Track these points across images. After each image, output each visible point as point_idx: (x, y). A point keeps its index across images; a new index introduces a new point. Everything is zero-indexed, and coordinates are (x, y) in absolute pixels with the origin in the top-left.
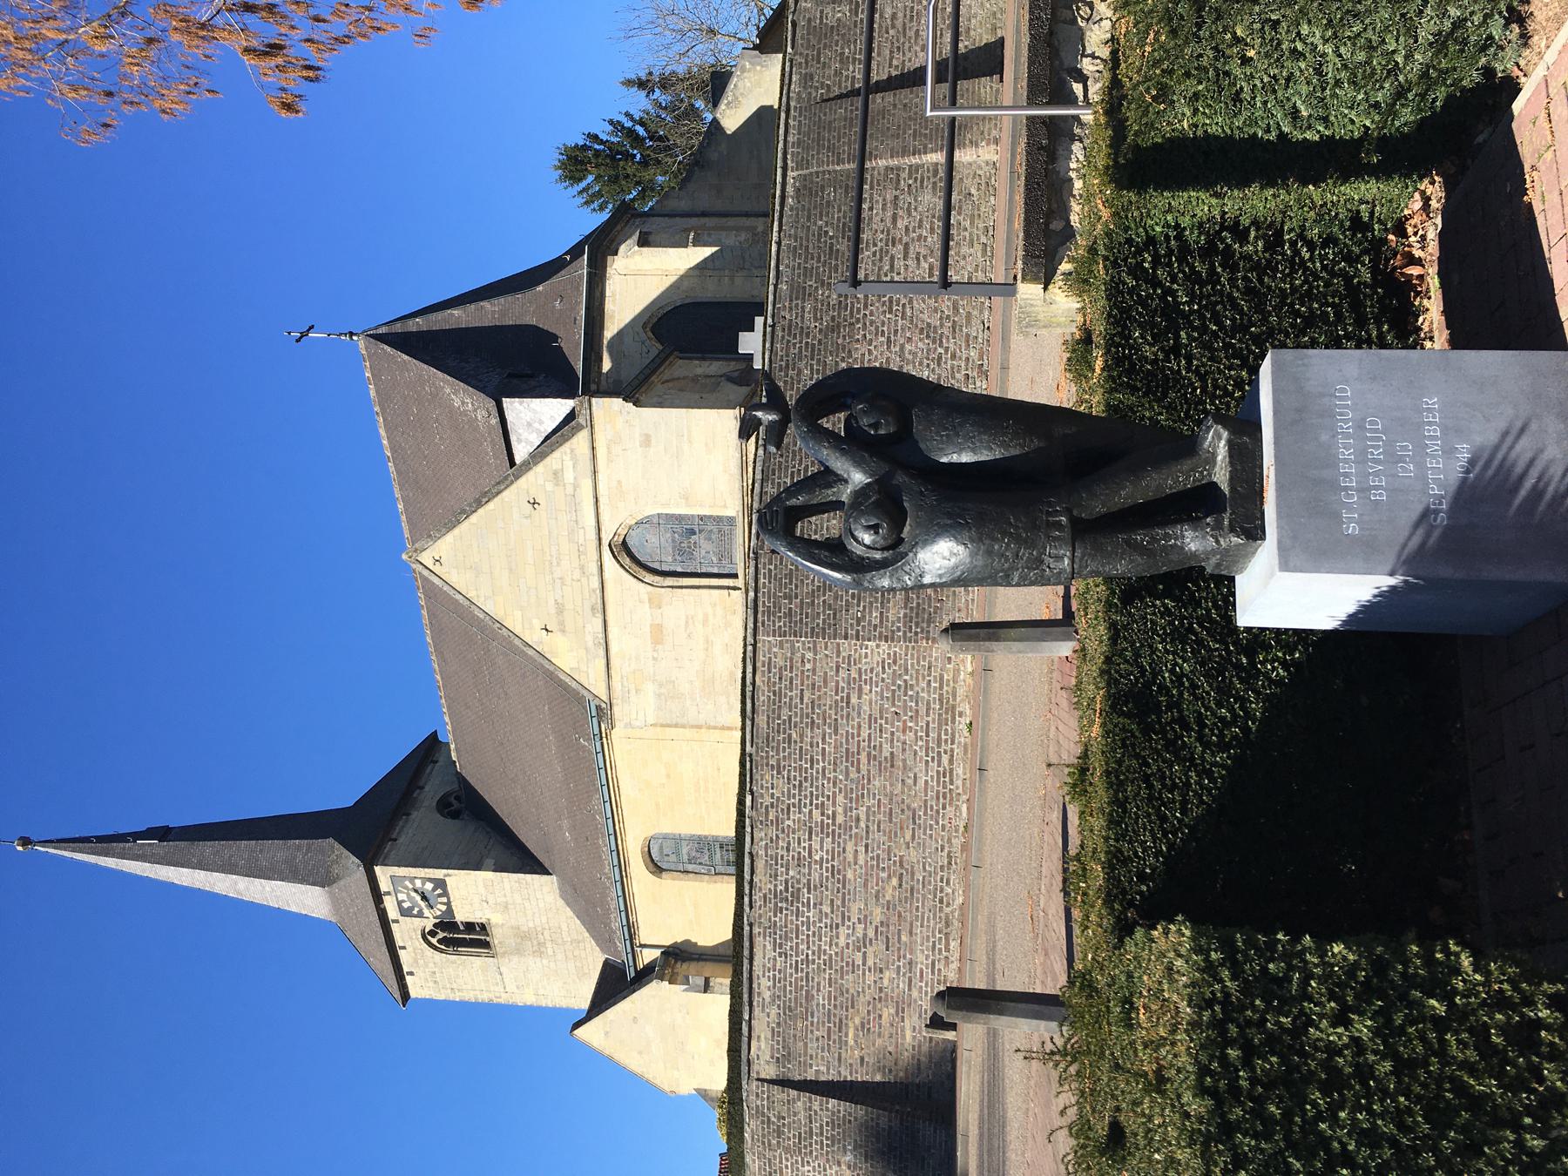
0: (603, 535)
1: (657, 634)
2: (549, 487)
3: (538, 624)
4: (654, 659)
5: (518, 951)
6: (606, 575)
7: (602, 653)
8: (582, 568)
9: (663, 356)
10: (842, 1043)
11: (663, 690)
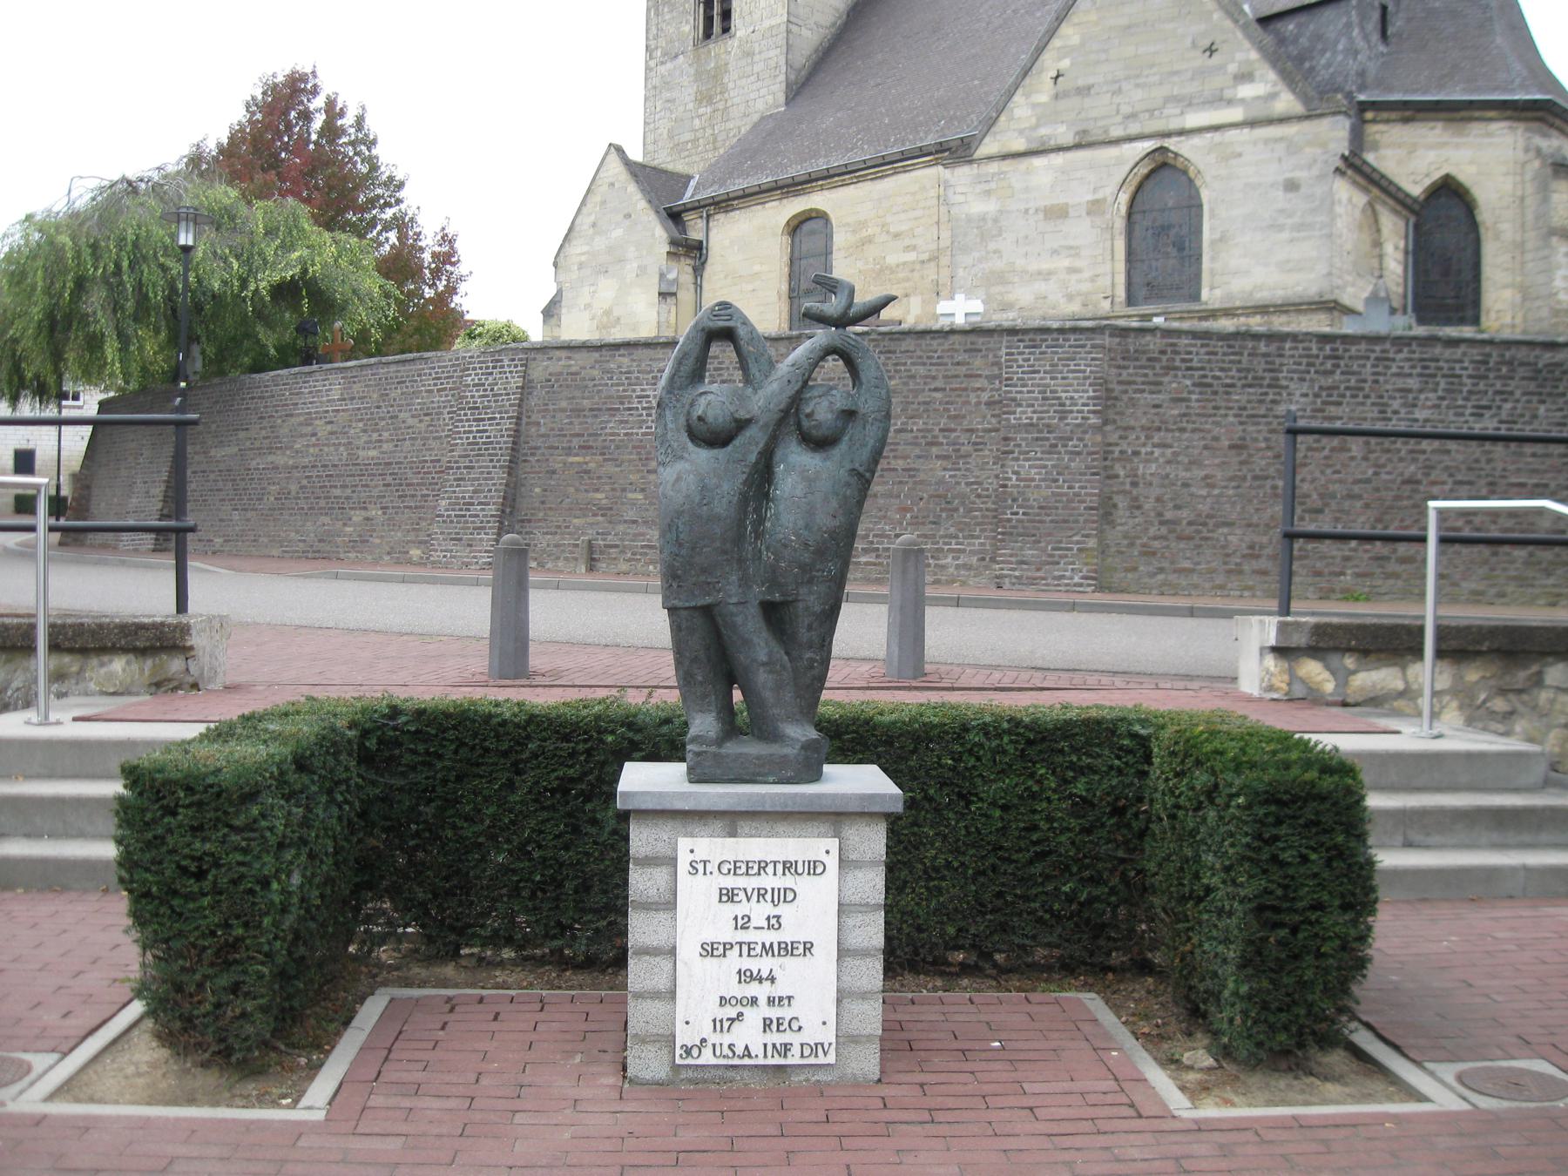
0: (1175, 139)
1: (1057, 213)
2: (1232, 68)
3: (1065, 64)
4: (1027, 211)
5: (698, 76)
6: (1126, 147)
7: (1034, 146)
8: (1133, 116)
9: (1409, 201)
10: (569, 451)
11: (990, 223)
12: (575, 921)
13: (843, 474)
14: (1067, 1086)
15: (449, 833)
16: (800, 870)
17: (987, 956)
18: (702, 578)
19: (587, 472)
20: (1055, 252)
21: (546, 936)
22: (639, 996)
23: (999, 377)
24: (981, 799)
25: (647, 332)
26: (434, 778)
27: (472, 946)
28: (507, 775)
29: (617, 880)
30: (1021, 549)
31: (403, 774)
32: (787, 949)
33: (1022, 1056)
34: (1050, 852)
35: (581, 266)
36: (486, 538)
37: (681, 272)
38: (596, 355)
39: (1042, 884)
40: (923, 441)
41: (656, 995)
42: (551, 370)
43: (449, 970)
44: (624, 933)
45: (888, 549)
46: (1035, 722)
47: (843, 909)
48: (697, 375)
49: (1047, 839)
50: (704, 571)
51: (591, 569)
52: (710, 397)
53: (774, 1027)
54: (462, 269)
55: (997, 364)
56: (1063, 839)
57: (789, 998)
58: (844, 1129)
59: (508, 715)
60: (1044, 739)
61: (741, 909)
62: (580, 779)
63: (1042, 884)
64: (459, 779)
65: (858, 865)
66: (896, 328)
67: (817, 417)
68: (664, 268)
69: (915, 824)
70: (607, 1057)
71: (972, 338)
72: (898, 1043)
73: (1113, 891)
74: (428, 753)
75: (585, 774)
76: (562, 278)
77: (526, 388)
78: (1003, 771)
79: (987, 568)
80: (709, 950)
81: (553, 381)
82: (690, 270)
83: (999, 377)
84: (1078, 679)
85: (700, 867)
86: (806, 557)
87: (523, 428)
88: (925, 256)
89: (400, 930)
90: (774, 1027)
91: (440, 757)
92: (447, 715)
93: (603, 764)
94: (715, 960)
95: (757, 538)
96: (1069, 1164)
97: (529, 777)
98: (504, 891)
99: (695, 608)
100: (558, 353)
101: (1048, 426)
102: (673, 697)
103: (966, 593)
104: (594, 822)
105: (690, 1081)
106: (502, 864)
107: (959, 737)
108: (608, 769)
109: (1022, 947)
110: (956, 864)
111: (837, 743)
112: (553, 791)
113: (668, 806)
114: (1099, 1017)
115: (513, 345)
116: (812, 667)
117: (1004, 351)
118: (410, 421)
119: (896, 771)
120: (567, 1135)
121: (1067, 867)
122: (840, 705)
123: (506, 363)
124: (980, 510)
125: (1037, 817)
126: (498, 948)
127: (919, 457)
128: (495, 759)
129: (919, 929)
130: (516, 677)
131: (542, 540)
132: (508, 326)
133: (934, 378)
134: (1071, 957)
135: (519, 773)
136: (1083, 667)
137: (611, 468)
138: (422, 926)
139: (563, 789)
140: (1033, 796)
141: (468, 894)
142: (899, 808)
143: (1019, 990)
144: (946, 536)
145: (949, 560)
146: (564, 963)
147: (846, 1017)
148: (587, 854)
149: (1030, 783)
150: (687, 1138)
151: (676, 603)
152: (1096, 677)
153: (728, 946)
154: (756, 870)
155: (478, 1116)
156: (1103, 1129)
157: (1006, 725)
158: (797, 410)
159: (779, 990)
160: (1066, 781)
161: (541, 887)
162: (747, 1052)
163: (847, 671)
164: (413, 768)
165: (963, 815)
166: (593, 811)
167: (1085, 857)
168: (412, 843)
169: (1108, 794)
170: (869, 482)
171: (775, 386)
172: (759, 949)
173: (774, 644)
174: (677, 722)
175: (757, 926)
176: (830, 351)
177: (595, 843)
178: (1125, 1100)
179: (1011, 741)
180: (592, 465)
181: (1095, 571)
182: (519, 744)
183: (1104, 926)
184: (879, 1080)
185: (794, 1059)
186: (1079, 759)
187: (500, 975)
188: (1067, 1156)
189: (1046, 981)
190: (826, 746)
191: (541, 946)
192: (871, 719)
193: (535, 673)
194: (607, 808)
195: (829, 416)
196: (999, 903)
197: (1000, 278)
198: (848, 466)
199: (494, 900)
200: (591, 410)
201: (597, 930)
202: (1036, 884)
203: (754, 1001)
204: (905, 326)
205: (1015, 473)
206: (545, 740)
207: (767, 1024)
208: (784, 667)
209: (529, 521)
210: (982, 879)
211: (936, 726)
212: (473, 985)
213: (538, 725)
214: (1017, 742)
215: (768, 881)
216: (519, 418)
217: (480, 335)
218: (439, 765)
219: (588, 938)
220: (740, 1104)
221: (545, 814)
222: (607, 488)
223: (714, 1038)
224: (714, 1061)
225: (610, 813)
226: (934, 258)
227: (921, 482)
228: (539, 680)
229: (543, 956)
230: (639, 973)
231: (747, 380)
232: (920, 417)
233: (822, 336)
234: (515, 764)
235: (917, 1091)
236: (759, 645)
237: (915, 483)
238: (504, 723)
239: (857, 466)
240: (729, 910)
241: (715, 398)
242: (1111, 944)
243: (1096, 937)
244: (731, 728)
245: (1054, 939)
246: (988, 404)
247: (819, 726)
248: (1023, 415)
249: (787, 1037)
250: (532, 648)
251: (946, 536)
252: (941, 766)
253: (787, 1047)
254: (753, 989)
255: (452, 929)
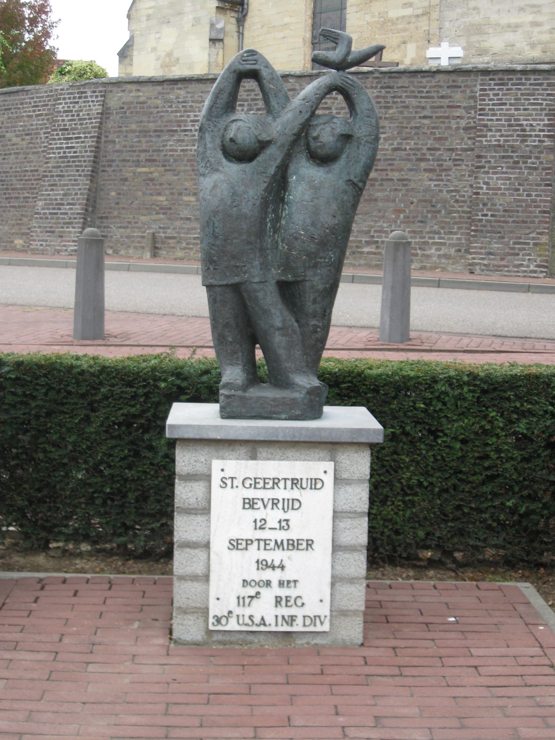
10: (138, 164)
12: (136, 523)
13: (341, 183)
14: (503, 651)
15: (41, 456)
16: (304, 485)
17: (448, 553)
18: (233, 263)
19: (152, 180)
20: (521, 9)
21: (114, 534)
22: (182, 578)
23: (474, 107)
24: (446, 435)
25: (200, 70)
26: (29, 414)
27: (57, 541)
28: (84, 412)
29: (167, 492)
30: (490, 243)
31: (6, 411)
32: (293, 545)
33: (471, 628)
34: (498, 476)
35: (149, 17)
36: (73, 231)
37: (227, 22)
38: (159, 88)
39: (491, 500)
40: (413, 157)
41: (195, 578)
42: (124, 100)
43: (41, 559)
44: (171, 533)
45: (383, 242)
46: (488, 376)
47: (337, 515)
48: (230, 106)
49: (496, 466)
50: (234, 257)
51: (155, 255)
52: (239, 124)
53: (283, 603)
54: (53, 17)
55: (473, 98)
56: (508, 465)
57: (295, 581)
58: (334, 679)
59: (85, 367)
60: (495, 389)
61: (259, 514)
62: (140, 416)
63: (491, 500)
64: (49, 414)
65: (348, 482)
66: (395, 69)
67: (321, 139)
68: (214, 20)
69: (395, 452)
70: (157, 624)
71: (454, 77)
72: (376, 616)
73: (545, 506)
74: (25, 395)
75: (144, 412)
76: (134, 27)
77: (105, 114)
78: (463, 413)
79: (462, 257)
80: (235, 544)
81: (124, 108)
82: (234, 21)
83: (474, 107)
84: (528, 344)
85: (229, 482)
86: (312, 247)
87: (102, 145)
88: (420, 12)
89: (4, 529)
90: (283, 603)
91: (34, 398)
92: (40, 366)
93: (158, 404)
94: (239, 552)
95: (275, 232)
96: (502, 708)
97: (101, 414)
98: (83, 500)
99: (227, 286)
100: (129, 86)
101: (512, 147)
102: (211, 354)
103: (445, 277)
104: (151, 448)
105: (220, 642)
106: (81, 480)
107: (430, 387)
108: (162, 408)
109: (476, 548)
110: (425, 484)
111: (336, 390)
112: (120, 424)
113: (205, 436)
114: (532, 600)
115: (95, 80)
116: (316, 332)
117: (479, 87)
118: (15, 140)
119: (381, 412)
120: (127, 681)
121: (511, 487)
122: (339, 361)
123: (89, 94)
124: (458, 212)
125: (488, 449)
126: (77, 542)
127: (411, 170)
128: (75, 400)
129: (397, 532)
130: (94, 339)
131: (117, 233)
132: (91, 65)
133: (423, 108)
134: (513, 555)
135: (94, 410)
136: (533, 335)
137: (170, 177)
138: (21, 526)
139: (127, 423)
140: (485, 432)
141: (55, 502)
142: (380, 439)
143: (472, 579)
144: (430, 232)
145: (433, 251)
146: (127, 555)
147: (338, 596)
148: (145, 472)
149: (483, 423)
150: (216, 684)
151: (213, 281)
152: (543, 343)
153: (249, 542)
154: (270, 485)
155: (61, 666)
156: (529, 683)
157: (466, 378)
158: (307, 134)
159: (287, 576)
160: (511, 422)
161: (110, 497)
162: (263, 622)
163: (349, 336)
164: (14, 406)
165: (432, 446)
166: (150, 440)
167: (524, 479)
168: (13, 463)
169: (543, 432)
170: (361, 190)
171: (290, 115)
172: (272, 544)
173: (286, 313)
174: (213, 372)
175: (271, 527)
176: (331, 89)
177: (152, 464)
178: (547, 662)
179: (470, 391)
180: (155, 175)
181: (547, 261)
182: (94, 388)
183: (538, 532)
184: (362, 644)
185: (298, 627)
186: (522, 405)
187: (79, 563)
188: (501, 702)
189: (493, 573)
190: (325, 391)
191: (110, 541)
192: (363, 372)
193: (110, 336)
194: (161, 438)
195: (331, 139)
196: (458, 514)
197: (478, 29)
198: (346, 178)
199: (76, 507)
200: (155, 131)
201: (152, 530)
202: (487, 500)
203: (268, 584)
204: (401, 67)
205: (485, 183)
206: (113, 386)
207: (278, 601)
208: (294, 331)
209: (107, 218)
210: (445, 496)
211: (411, 378)
212: (59, 570)
213: (108, 374)
214: (474, 391)
215: (280, 493)
216: (99, 138)
217: (69, 72)
218: (33, 404)
219: (146, 536)
220: (257, 660)
221: (114, 442)
222: (167, 192)
223: (238, 611)
224: (238, 628)
225: (163, 442)
226: (426, 13)
227: (413, 190)
228: (113, 341)
229: (112, 549)
230: (181, 561)
231: (269, 109)
232: (412, 139)
233: (329, 76)
234: (91, 404)
235: (391, 652)
236: (275, 314)
237: (407, 190)
238: (82, 372)
239: (352, 177)
240: (251, 515)
241: (244, 124)
242: (543, 546)
243: (532, 541)
244: (254, 377)
245: (500, 541)
246: (466, 129)
247: (321, 377)
248: (492, 138)
249: (293, 611)
250: (107, 316)
251: (430, 232)
252: (416, 409)
253: (293, 618)
254: (268, 574)
255: (44, 528)
